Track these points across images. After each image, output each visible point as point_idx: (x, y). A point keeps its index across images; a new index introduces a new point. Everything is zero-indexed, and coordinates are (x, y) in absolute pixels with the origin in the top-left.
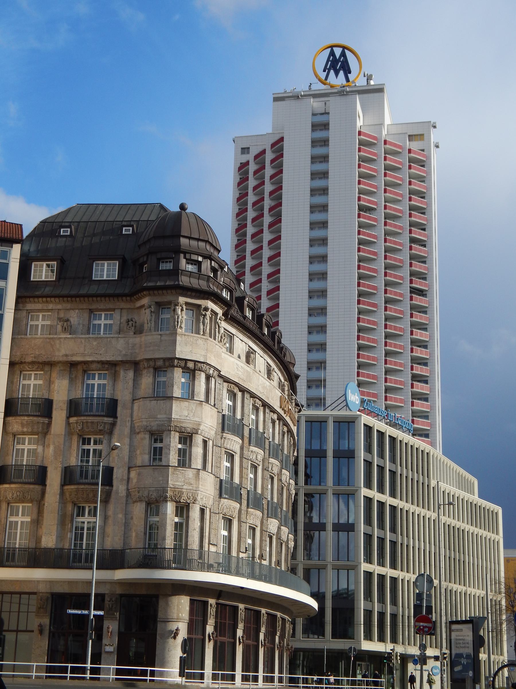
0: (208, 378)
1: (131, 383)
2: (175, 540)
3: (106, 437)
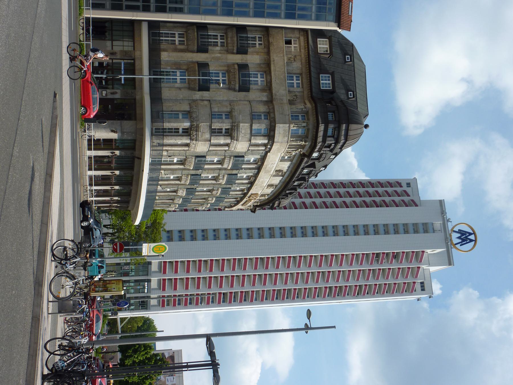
0: (265, 145)
1: (260, 99)
2: (169, 129)
3: (227, 86)
